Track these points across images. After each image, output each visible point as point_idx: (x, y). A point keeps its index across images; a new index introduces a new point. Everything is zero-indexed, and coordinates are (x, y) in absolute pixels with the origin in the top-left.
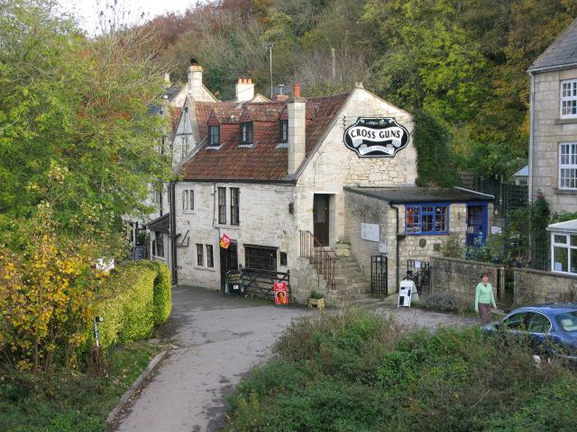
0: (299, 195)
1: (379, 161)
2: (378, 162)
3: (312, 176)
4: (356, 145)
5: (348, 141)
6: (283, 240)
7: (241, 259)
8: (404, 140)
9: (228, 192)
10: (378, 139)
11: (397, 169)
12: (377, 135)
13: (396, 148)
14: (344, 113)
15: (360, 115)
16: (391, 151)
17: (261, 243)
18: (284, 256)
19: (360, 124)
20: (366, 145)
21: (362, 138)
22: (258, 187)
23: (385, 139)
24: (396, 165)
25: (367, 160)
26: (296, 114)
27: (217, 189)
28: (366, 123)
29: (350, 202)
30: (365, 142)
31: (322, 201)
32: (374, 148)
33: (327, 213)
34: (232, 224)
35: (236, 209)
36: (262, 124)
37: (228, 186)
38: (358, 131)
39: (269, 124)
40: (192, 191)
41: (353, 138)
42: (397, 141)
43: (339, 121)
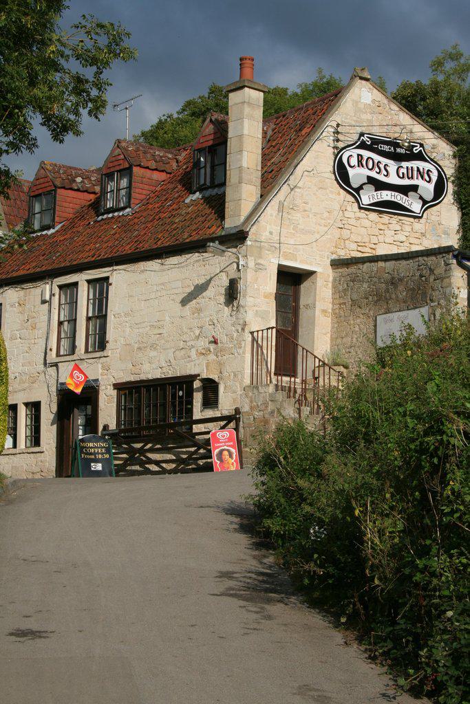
0: (251, 264)
2: (391, 221)
3: (276, 229)
4: (355, 185)
5: (342, 173)
6: (212, 357)
7: (108, 414)
8: (439, 190)
9: (83, 292)
10: (393, 179)
12: (392, 173)
13: (425, 202)
14: (336, 117)
15: (364, 130)
16: (416, 207)
17: (157, 374)
18: (211, 388)
19: (363, 146)
20: (372, 187)
22: (154, 265)
23: (406, 182)
24: (423, 235)
25: (373, 216)
27: (56, 290)
28: (373, 145)
29: (340, 291)
30: (371, 180)
31: (291, 279)
32: (386, 195)
33: (296, 311)
34: (87, 351)
35: (100, 317)
36: (148, 173)
37: (81, 278)
38: (360, 156)
39: (163, 176)
41: (351, 172)
42: (428, 189)
43: (327, 132)
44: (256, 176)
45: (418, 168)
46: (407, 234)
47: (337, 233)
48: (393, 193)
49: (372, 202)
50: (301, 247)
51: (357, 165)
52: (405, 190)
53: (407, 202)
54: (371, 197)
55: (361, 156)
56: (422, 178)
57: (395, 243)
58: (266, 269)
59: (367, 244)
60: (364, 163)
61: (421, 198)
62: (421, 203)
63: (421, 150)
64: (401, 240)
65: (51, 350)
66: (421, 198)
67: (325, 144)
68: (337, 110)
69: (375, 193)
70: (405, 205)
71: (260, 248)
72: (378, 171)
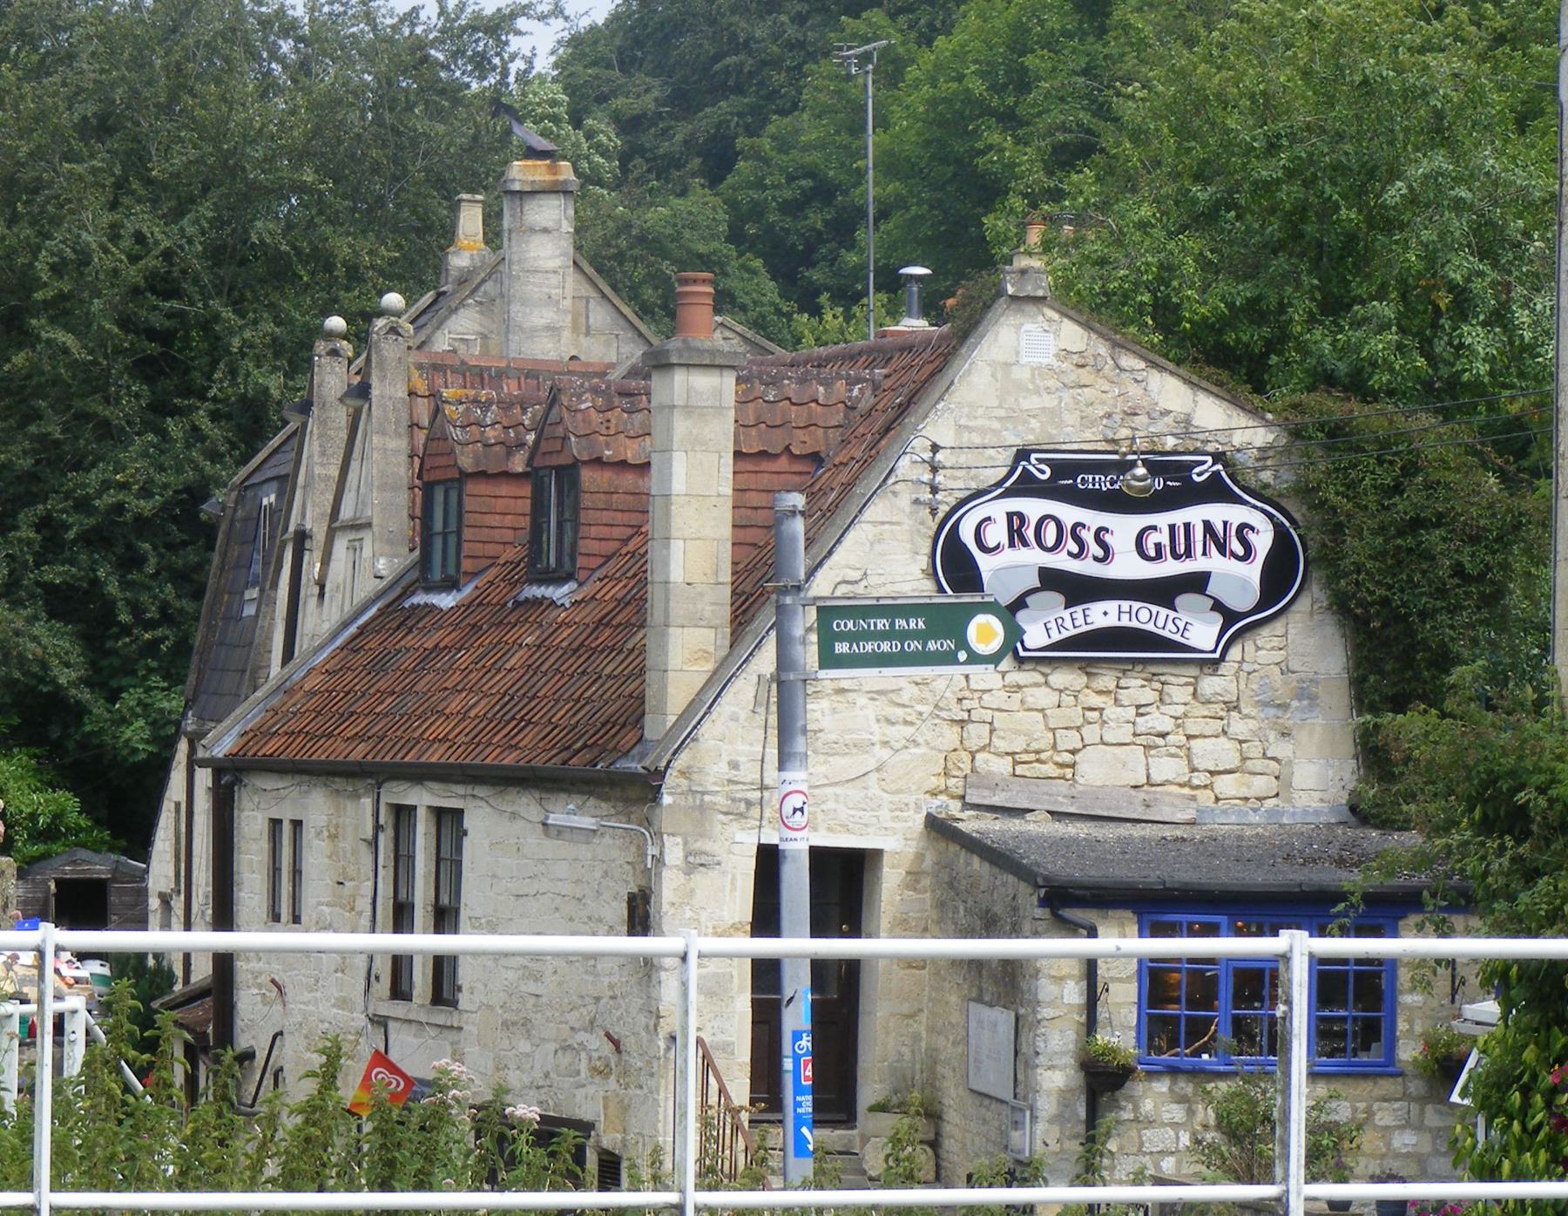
0: (674, 852)
1: (1137, 689)
9: (423, 828)
10: (1127, 566)
11: (1239, 727)
16: (1203, 632)
19: (1027, 486)
21: (1033, 557)
23: (1169, 568)
26: (681, 427)
30: (1051, 579)
32: (1103, 614)
34: (1307, 1199)
37: (422, 798)
38: (1016, 525)
40: (297, 824)
41: (984, 562)
44: (717, 602)
45: (1208, 526)
46: (1180, 710)
47: (951, 736)
48: (1125, 605)
49: (1056, 637)
50: (829, 791)
51: (1005, 540)
52: (1162, 592)
53: (1170, 625)
54: (1052, 625)
55: (1021, 516)
56: (1222, 548)
57: (1138, 740)
58: (719, 864)
59: (1043, 756)
60: (1030, 533)
61: (1218, 606)
62: (1218, 620)
63: (1216, 474)
64: (1161, 728)
65: (377, 978)
66: (1218, 606)
67: (904, 501)
68: (941, 398)
69: (1066, 614)
70: (1165, 633)
71: (702, 808)
72: (1075, 549)
